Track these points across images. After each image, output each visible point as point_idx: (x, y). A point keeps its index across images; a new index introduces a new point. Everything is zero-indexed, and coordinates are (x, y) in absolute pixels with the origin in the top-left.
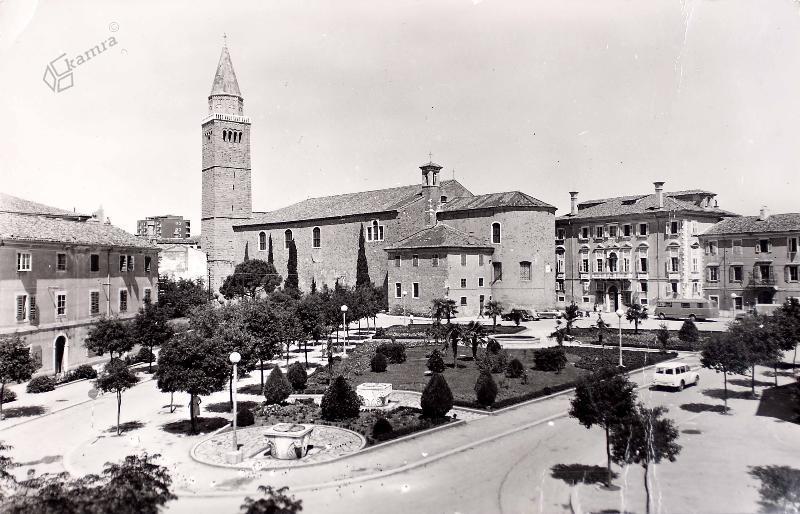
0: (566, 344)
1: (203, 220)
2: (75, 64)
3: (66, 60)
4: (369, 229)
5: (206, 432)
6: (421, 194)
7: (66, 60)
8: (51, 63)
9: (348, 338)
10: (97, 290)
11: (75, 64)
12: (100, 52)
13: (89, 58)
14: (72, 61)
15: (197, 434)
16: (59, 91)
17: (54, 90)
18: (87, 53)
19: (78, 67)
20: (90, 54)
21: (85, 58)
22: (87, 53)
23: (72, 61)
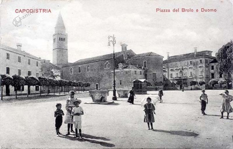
0: (47, 94)
1: (21, 46)
2: (22, 18)
3: (19, 18)
4: (105, 65)
5: (205, 110)
6: (198, 117)
7: (19, 18)
8: (15, 18)
9: (88, 89)
10: (20, 69)
11: (22, 18)
12: (29, 15)
13: (26, 17)
14: (21, 18)
15: (201, 109)
16: (17, 26)
17: (16, 26)
18: (25, 15)
19: (23, 19)
20: (26, 16)
21: (25, 17)
22: (25, 15)
23: (21, 18)
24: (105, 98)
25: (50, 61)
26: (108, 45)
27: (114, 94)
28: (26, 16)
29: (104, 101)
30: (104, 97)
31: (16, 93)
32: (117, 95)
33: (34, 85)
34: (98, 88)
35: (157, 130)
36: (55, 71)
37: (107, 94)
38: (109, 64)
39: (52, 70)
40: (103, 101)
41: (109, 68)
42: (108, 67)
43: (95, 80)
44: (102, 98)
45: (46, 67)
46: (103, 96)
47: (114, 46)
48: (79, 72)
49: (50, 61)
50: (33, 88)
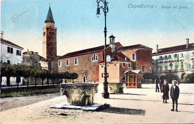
2: (19, 16)
24: (91, 98)
25: (38, 53)
26: (97, 13)
27: (106, 89)
28: (21, 14)
29: (90, 104)
30: (89, 96)
31: (18, 84)
32: (109, 91)
33: (14, 76)
34: (86, 81)
35: (129, 110)
36: (43, 63)
37: (94, 89)
38: (97, 56)
39: (40, 62)
40: (86, 103)
41: (96, 61)
42: (96, 59)
43: (82, 73)
44: (86, 97)
45: (33, 57)
46: (87, 94)
47: (105, 15)
48: (67, 65)
49: (38, 53)
50: (13, 80)
